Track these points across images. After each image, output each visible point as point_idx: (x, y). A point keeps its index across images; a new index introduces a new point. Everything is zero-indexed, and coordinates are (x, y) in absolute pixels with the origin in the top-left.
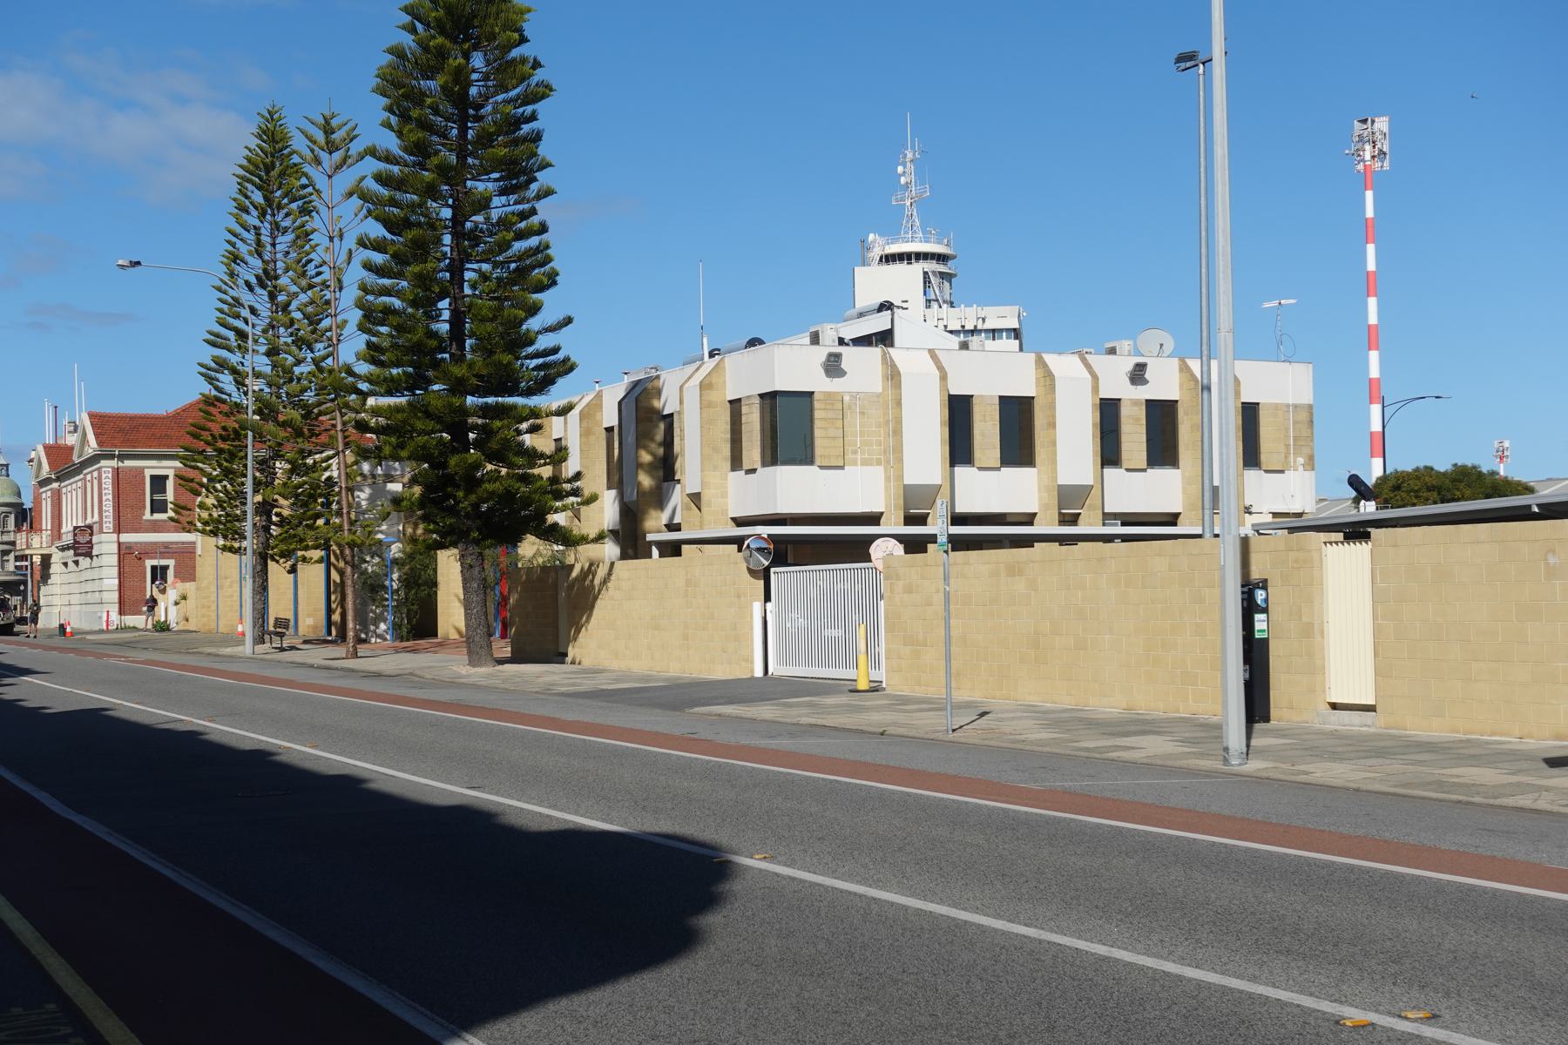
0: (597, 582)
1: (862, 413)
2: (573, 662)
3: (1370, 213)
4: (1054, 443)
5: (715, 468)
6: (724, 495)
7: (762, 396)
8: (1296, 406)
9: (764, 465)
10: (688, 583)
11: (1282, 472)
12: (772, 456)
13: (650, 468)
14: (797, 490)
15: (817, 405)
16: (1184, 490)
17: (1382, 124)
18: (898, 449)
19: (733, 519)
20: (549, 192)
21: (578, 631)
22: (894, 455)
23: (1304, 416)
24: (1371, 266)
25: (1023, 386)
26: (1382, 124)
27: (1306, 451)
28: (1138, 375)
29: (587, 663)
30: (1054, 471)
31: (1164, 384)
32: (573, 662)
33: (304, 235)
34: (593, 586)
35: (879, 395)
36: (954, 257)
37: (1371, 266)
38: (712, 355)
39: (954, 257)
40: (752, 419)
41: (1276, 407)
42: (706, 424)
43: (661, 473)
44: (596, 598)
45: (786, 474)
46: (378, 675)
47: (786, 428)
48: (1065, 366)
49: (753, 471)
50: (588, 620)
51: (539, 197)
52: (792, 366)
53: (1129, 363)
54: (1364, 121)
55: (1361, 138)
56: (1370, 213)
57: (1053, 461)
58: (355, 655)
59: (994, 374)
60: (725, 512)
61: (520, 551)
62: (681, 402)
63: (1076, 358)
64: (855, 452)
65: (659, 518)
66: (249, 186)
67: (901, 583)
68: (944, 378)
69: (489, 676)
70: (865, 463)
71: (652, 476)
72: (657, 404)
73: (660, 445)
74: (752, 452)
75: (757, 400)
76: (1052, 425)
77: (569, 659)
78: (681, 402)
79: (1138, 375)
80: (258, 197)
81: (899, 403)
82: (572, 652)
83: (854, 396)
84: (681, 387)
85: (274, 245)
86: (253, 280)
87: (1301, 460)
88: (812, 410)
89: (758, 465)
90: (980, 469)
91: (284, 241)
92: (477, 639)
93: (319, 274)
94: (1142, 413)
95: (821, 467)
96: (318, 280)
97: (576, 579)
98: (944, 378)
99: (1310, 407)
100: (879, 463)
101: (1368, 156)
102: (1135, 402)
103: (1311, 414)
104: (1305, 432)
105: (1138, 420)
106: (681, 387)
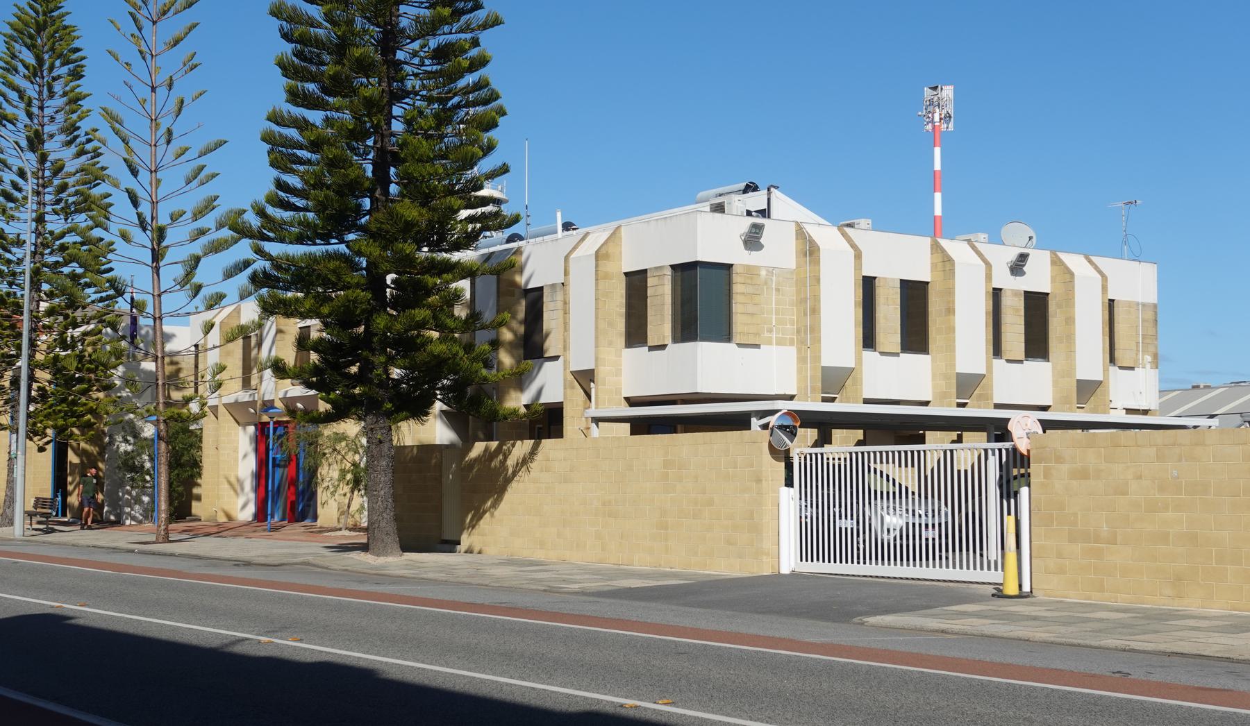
0: (511, 462)
1: (777, 290)
2: (469, 551)
3: (937, 166)
4: (951, 330)
5: (610, 344)
6: (618, 373)
7: (673, 267)
8: (1144, 305)
9: (675, 340)
10: (667, 464)
11: (1132, 368)
12: (687, 329)
13: (512, 347)
14: (711, 368)
15: (735, 278)
16: (1055, 383)
17: (948, 92)
18: (815, 329)
19: (627, 399)
20: (495, 22)
21: (478, 517)
22: (808, 334)
23: (1150, 315)
24: (938, 211)
25: (920, 272)
26: (948, 92)
27: (1152, 349)
28: (1018, 267)
29: (492, 551)
30: (953, 359)
31: (1038, 278)
32: (469, 551)
33: (75, 100)
34: (506, 469)
35: (792, 272)
36: (506, 201)
37: (938, 211)
38: (567, 226)
39: (506, 201)
40: (661, 295)
41: (1130, 304)
42: (600, 298)
43: (521, 352)
44: (508, 481)
45: (706, 351)
46: (115, 550)
47: (701, 301)
48: (956, 249)
49: (663, 347)
50: (495, 505)
51: (485, 26)
52: (715, 239)
53: (1012, 254)
54: (935, 88)
55: (931, 103)
56: (937, 166)
57: (950, 348)
58: (167, 540)
59: (900, 257)
60: (619, 391)
61: (404, 425)
62: (566, 273)
63: (965, 245)
64: (770, 331)
65: (518, 399)
66: (17, 46)
67: (1065, 468)
68: (858, 256)
69: (407, 566)
70: (780, 342)
71: (513, 356)
72: (521, 280)
73: (521, 323)
74: (660, 322)
75: (669, 272)
76: (950, 311)
77: (463, 547)
78: (566, 273)
79: (1018, 267)
80: (29, 58)
81: (817, 280)
82: (466, 540)
83: (770, 271)
84: (567, 258)
85: (41, 108)
86: (24, 143)
87: (1148, 358)
88: (729, 283)
89: (668, 341)
90: (882, 353)
91: (59, 102)
92: (383, 524)
93: (89, 141)
94: (1020, 304)
95: (739, 345)
96: (89, 147)
97: (476, 460)
98: (858, 256)
99: (1155, 306)
100: (792, 344)
101: (937, 118)
102: (1015, 293)
103: (1156, 313)
104: (1151, 331)
105: (1017, 310)
106: (567, 258)
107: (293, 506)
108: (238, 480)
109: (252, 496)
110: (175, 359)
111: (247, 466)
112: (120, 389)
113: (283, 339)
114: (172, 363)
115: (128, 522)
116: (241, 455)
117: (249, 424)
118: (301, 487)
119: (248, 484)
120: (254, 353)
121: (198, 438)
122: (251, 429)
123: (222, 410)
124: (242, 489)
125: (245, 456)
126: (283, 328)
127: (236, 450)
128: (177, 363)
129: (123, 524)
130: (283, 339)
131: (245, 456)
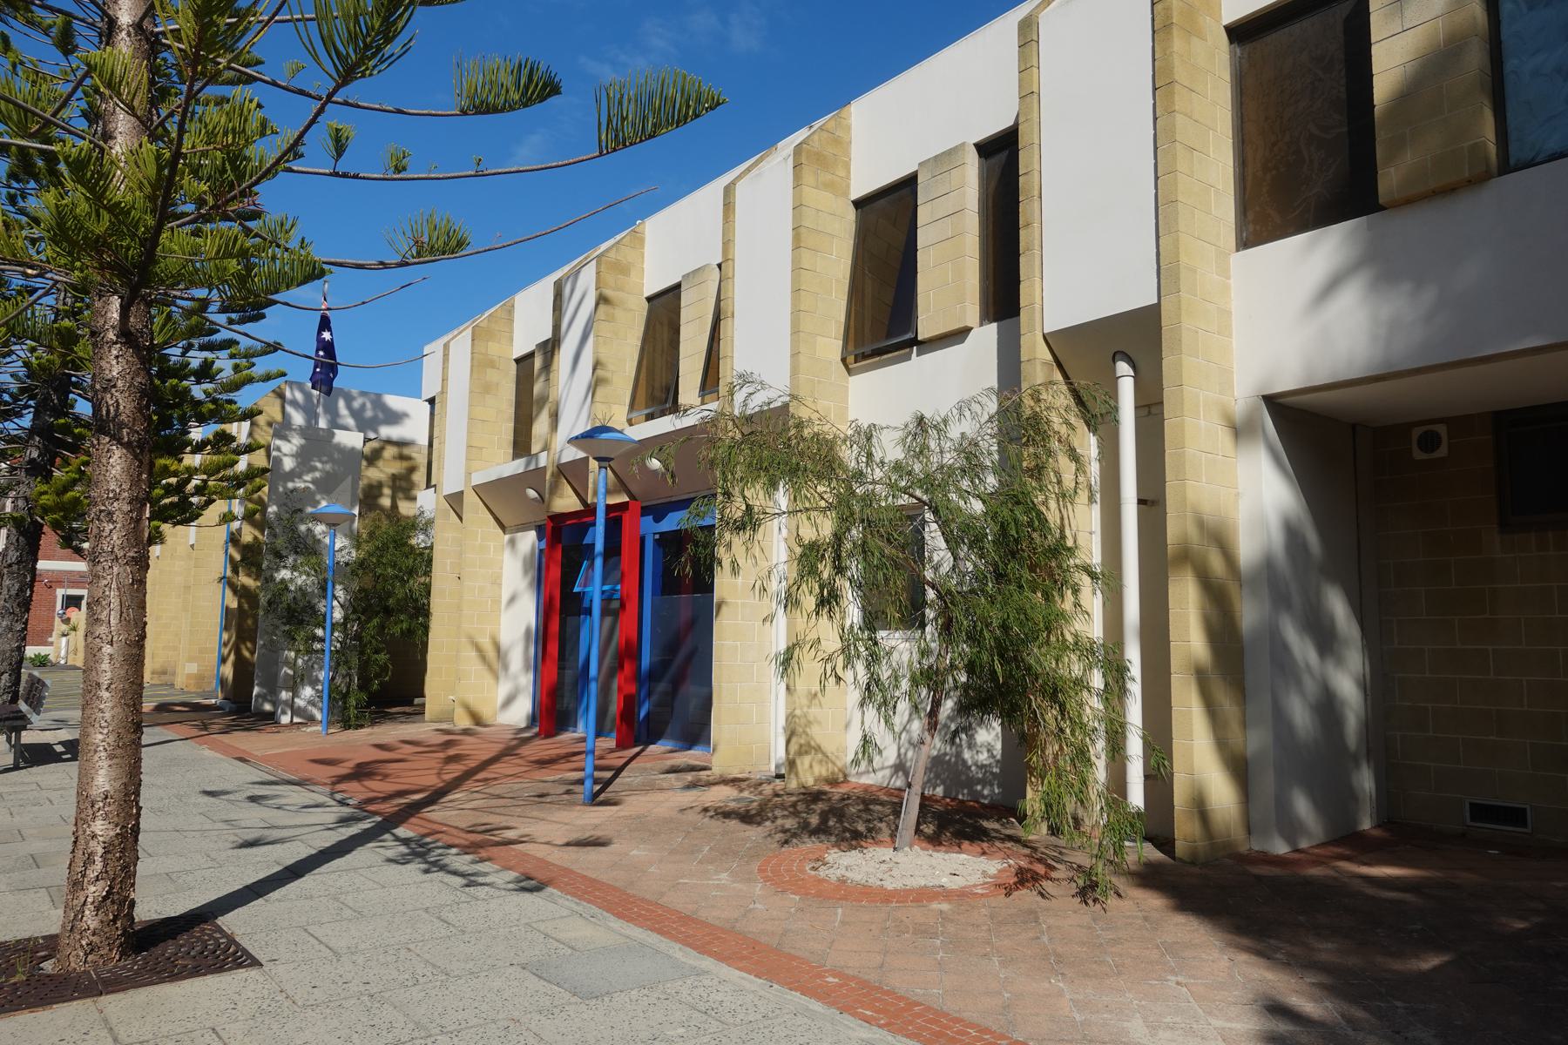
107: (630, 706)
108: (497, 647)
109: (526, 680)
110: (406, 451)
111: (516, 616)
112: (292, 475)
113: (610, 319)
114: (402, 457)
115: (285, 719)
116: (505, 598)
117: (523, 528)
118: (646, 661)
119: (518, 656)
120: (537, 388)
121: (425, 560)
122: (528, 540)
123: (471, 499)
124: (506, 667)
125: (512, 600)
126: (608, 292)
127: (497, 582)
128: (409, 458)
129: (277, 722)
130: (610, 319)
131: (512, 600)
